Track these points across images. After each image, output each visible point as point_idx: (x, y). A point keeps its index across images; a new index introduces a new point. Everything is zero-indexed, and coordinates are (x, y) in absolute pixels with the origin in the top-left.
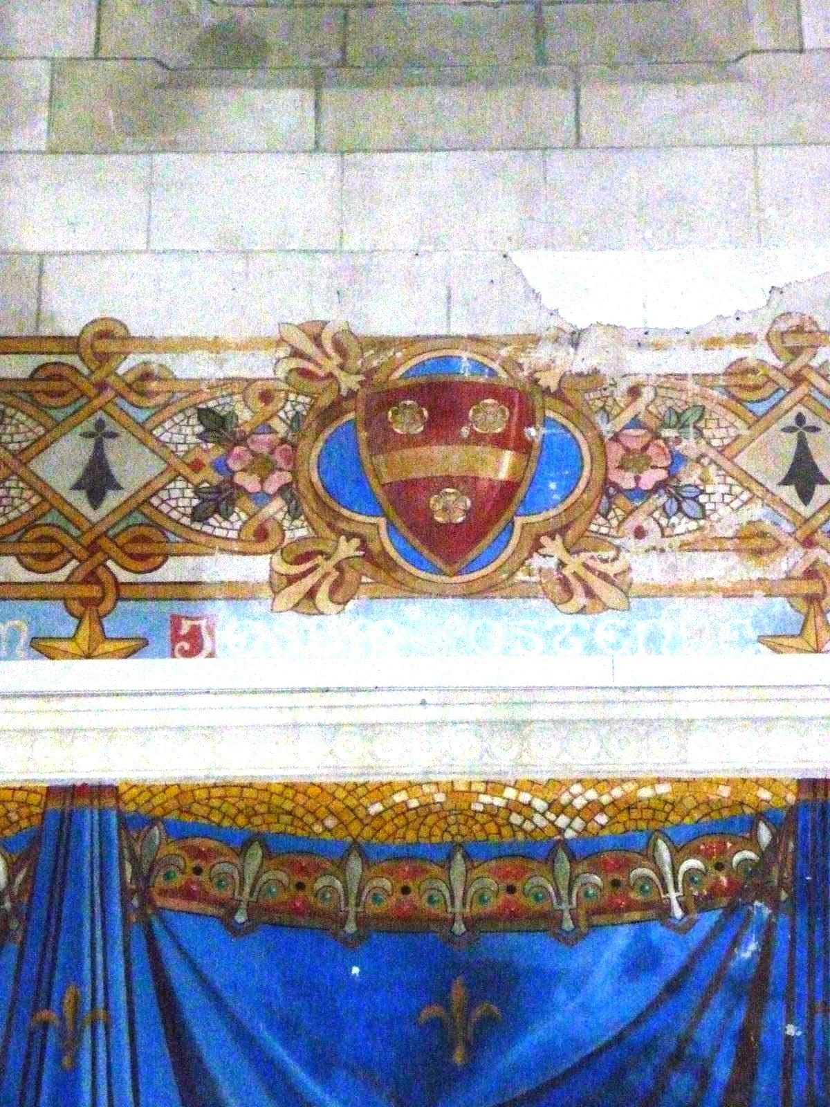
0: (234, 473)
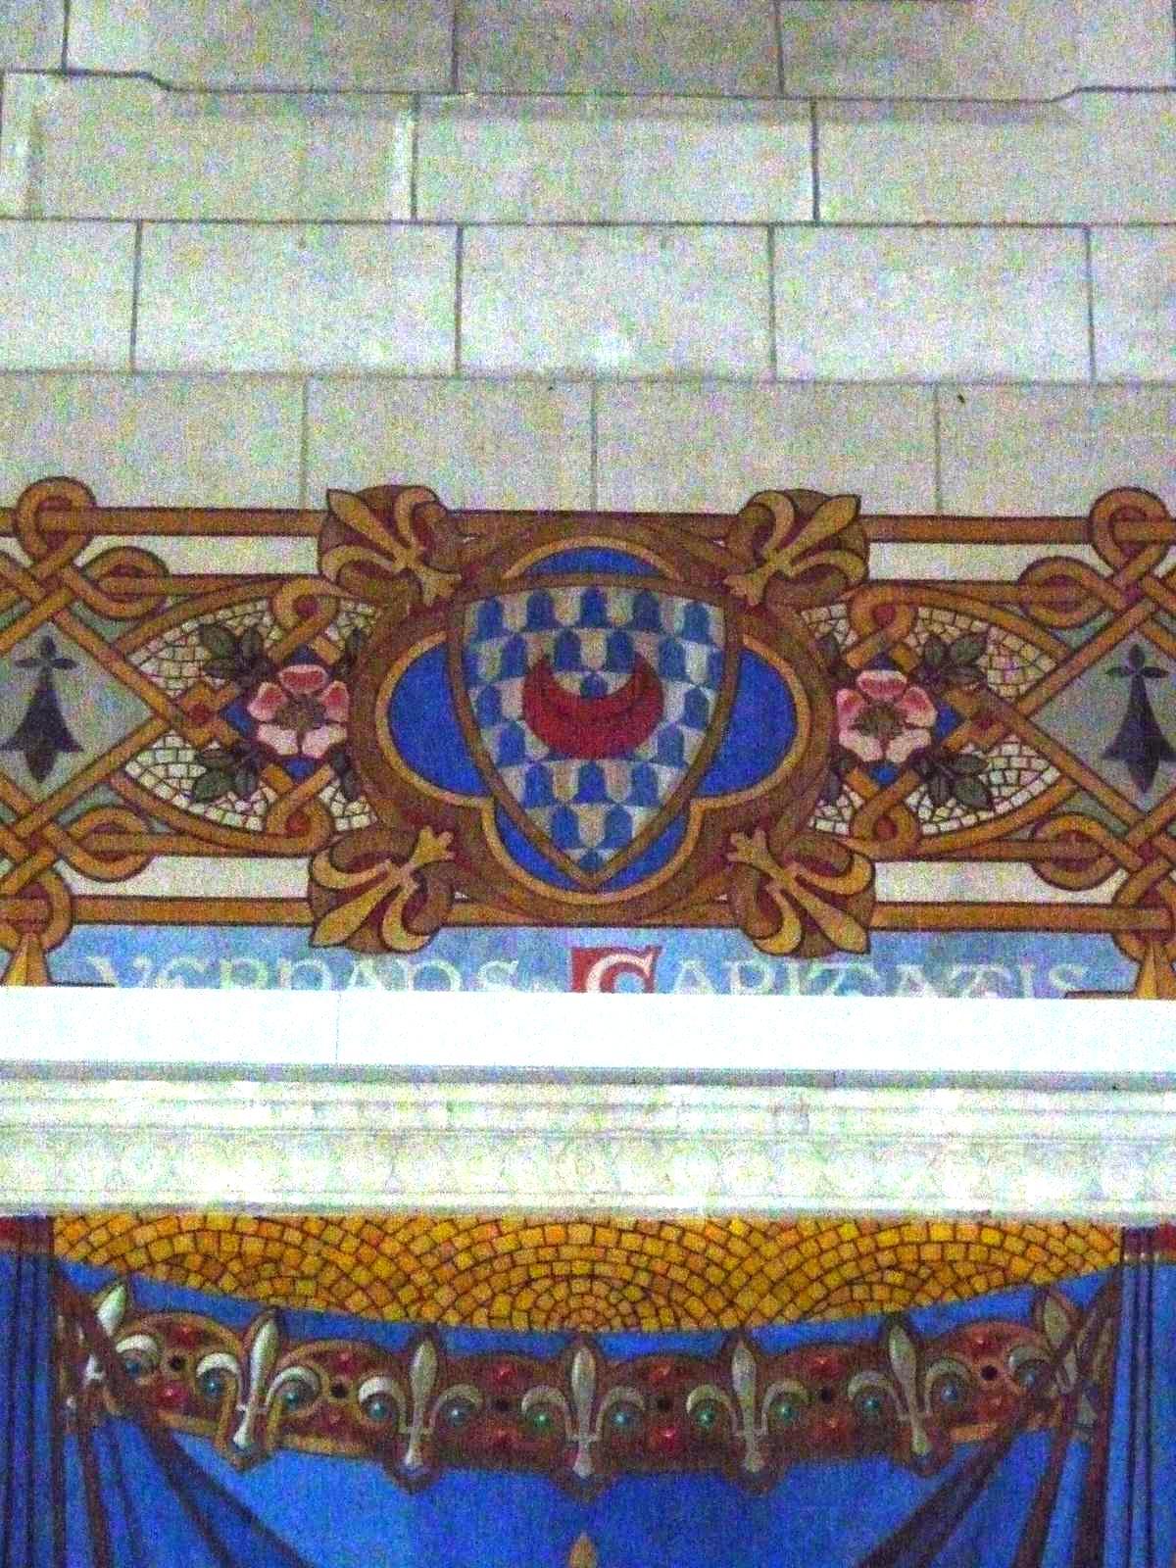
0: (256, 723)
